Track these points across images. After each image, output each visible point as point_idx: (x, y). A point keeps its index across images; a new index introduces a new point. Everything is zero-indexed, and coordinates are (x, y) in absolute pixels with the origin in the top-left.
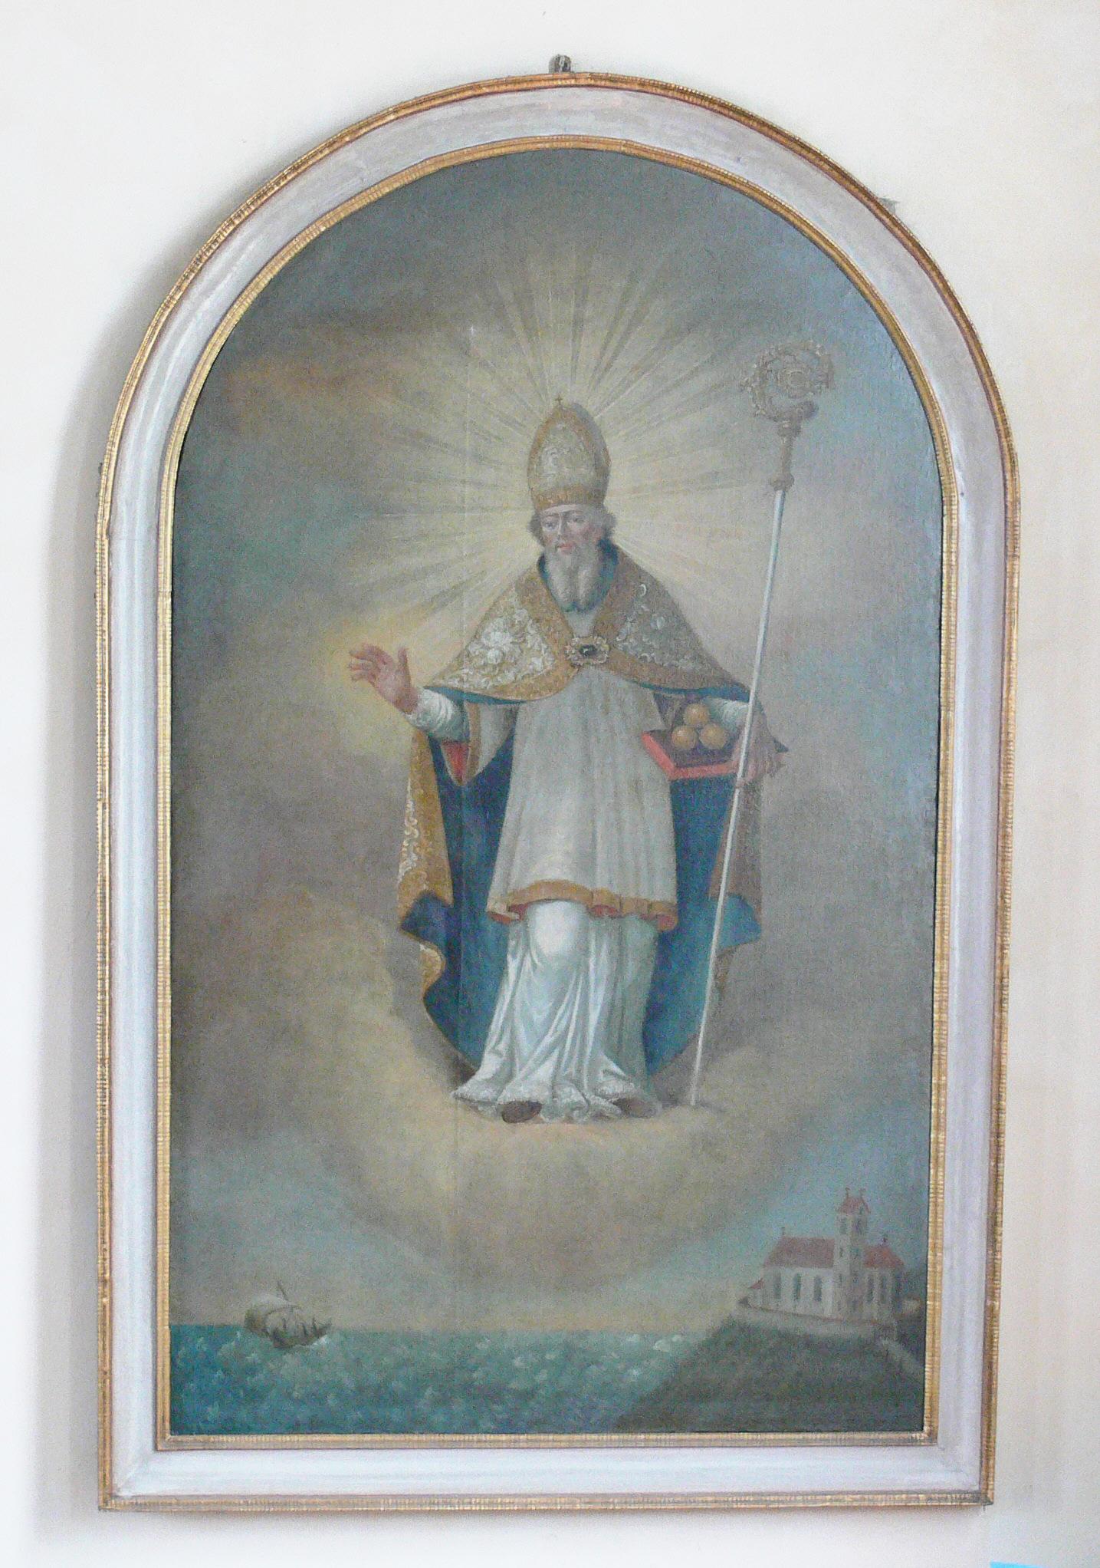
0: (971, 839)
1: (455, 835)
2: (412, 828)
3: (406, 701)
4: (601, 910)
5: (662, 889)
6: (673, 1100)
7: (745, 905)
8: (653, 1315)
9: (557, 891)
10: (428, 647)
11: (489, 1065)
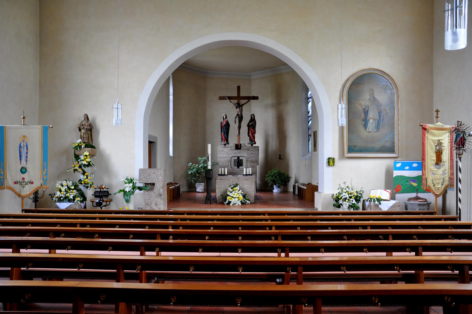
0: (5, 283)
1: (365, 114)
3: (362, 106)
4: (374, 119)
5: (378, 118)
6: (379, 131)
9: (371, 118)
10: (363, 103)
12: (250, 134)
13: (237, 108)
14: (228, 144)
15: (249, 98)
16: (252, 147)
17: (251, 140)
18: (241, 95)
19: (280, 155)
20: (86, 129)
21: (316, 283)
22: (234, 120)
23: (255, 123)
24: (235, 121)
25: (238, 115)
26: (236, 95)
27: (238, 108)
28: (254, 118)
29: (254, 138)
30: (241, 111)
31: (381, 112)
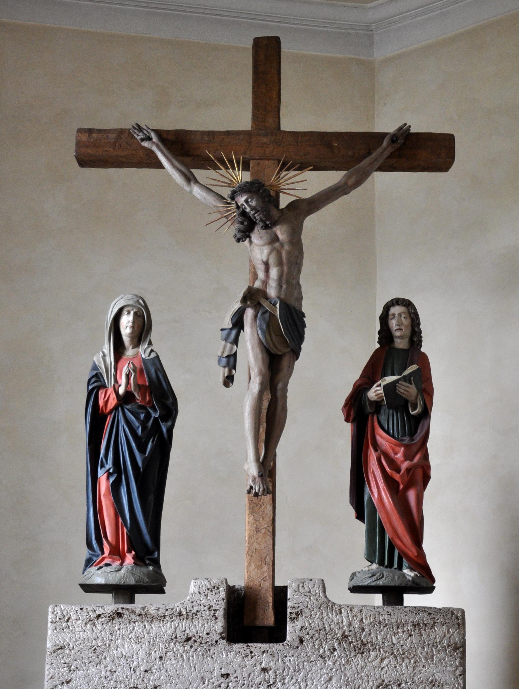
12: (377, 490)
13: (245, 233)
14: (156, 585)
15: (359, 154)
16: (395, 614)
17: (381, 548)
18: (287, 124)
21: (268, 361)
22: (220, 347)
23: (423, 380)
24: (231, 361)
25: (253, 297)
26: (236, 114)
27: (258, 237)
29: (416, 531)
30: (291, 262)
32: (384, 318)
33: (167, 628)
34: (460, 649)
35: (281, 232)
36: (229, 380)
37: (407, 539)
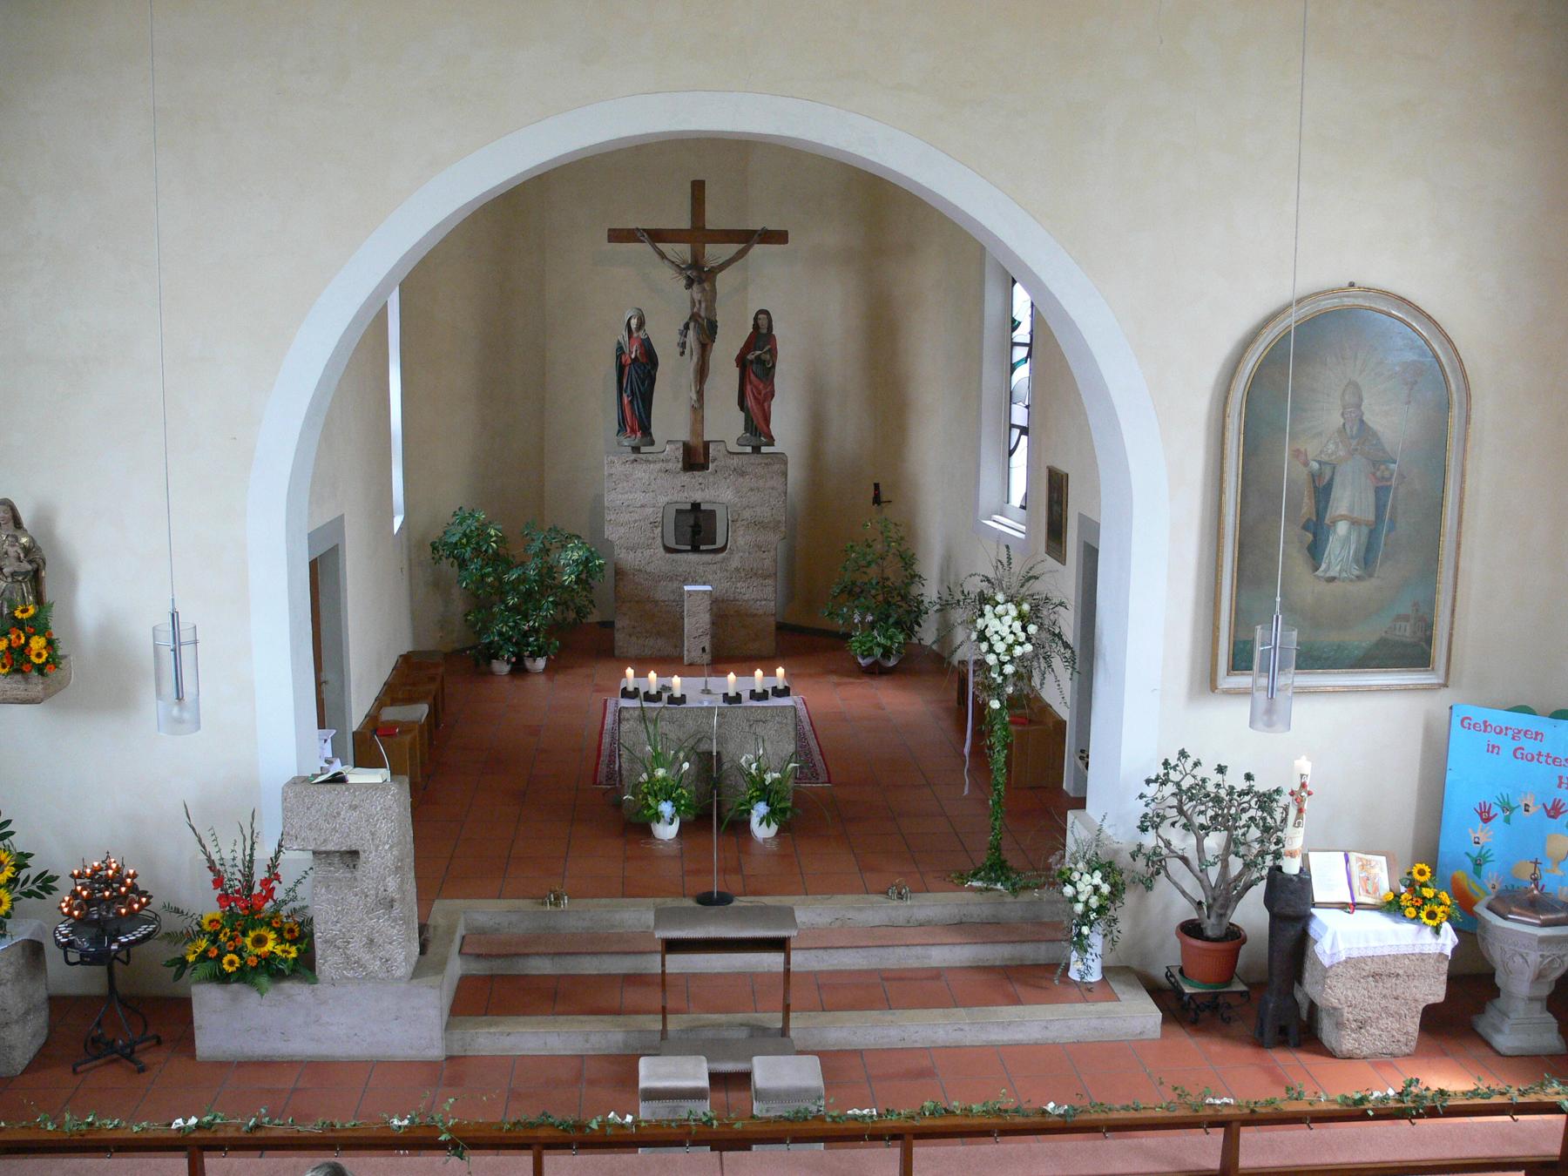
1: (1317, 503)
2: (1306, 500)
3: (1306, 464)
4: (1354, 523)
5: (1371, 517)
6: (1371, 576)
7: (1393, 521)
8: (1362, 636)
10: (1311, 448)
11: (1323, 566)
15: (747, 238)
16: (755, 459)
19: (877, 486)
20: (13, 574)
22: (677, 338)
23: (773, 352)
24: (683, 345)
25: (694, 317)
27: (695, 287)
28: (770, 328)
29: (767, 420)
31: (1388, 488)
32: (756, 319)
33: (658, 466)
34: (785, 474)
35: (706, 286)
36: (682, 353)
37: (761, 420)
